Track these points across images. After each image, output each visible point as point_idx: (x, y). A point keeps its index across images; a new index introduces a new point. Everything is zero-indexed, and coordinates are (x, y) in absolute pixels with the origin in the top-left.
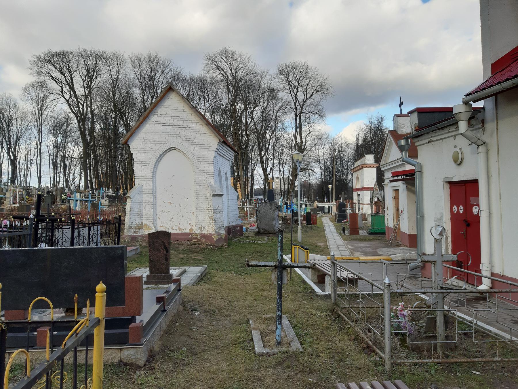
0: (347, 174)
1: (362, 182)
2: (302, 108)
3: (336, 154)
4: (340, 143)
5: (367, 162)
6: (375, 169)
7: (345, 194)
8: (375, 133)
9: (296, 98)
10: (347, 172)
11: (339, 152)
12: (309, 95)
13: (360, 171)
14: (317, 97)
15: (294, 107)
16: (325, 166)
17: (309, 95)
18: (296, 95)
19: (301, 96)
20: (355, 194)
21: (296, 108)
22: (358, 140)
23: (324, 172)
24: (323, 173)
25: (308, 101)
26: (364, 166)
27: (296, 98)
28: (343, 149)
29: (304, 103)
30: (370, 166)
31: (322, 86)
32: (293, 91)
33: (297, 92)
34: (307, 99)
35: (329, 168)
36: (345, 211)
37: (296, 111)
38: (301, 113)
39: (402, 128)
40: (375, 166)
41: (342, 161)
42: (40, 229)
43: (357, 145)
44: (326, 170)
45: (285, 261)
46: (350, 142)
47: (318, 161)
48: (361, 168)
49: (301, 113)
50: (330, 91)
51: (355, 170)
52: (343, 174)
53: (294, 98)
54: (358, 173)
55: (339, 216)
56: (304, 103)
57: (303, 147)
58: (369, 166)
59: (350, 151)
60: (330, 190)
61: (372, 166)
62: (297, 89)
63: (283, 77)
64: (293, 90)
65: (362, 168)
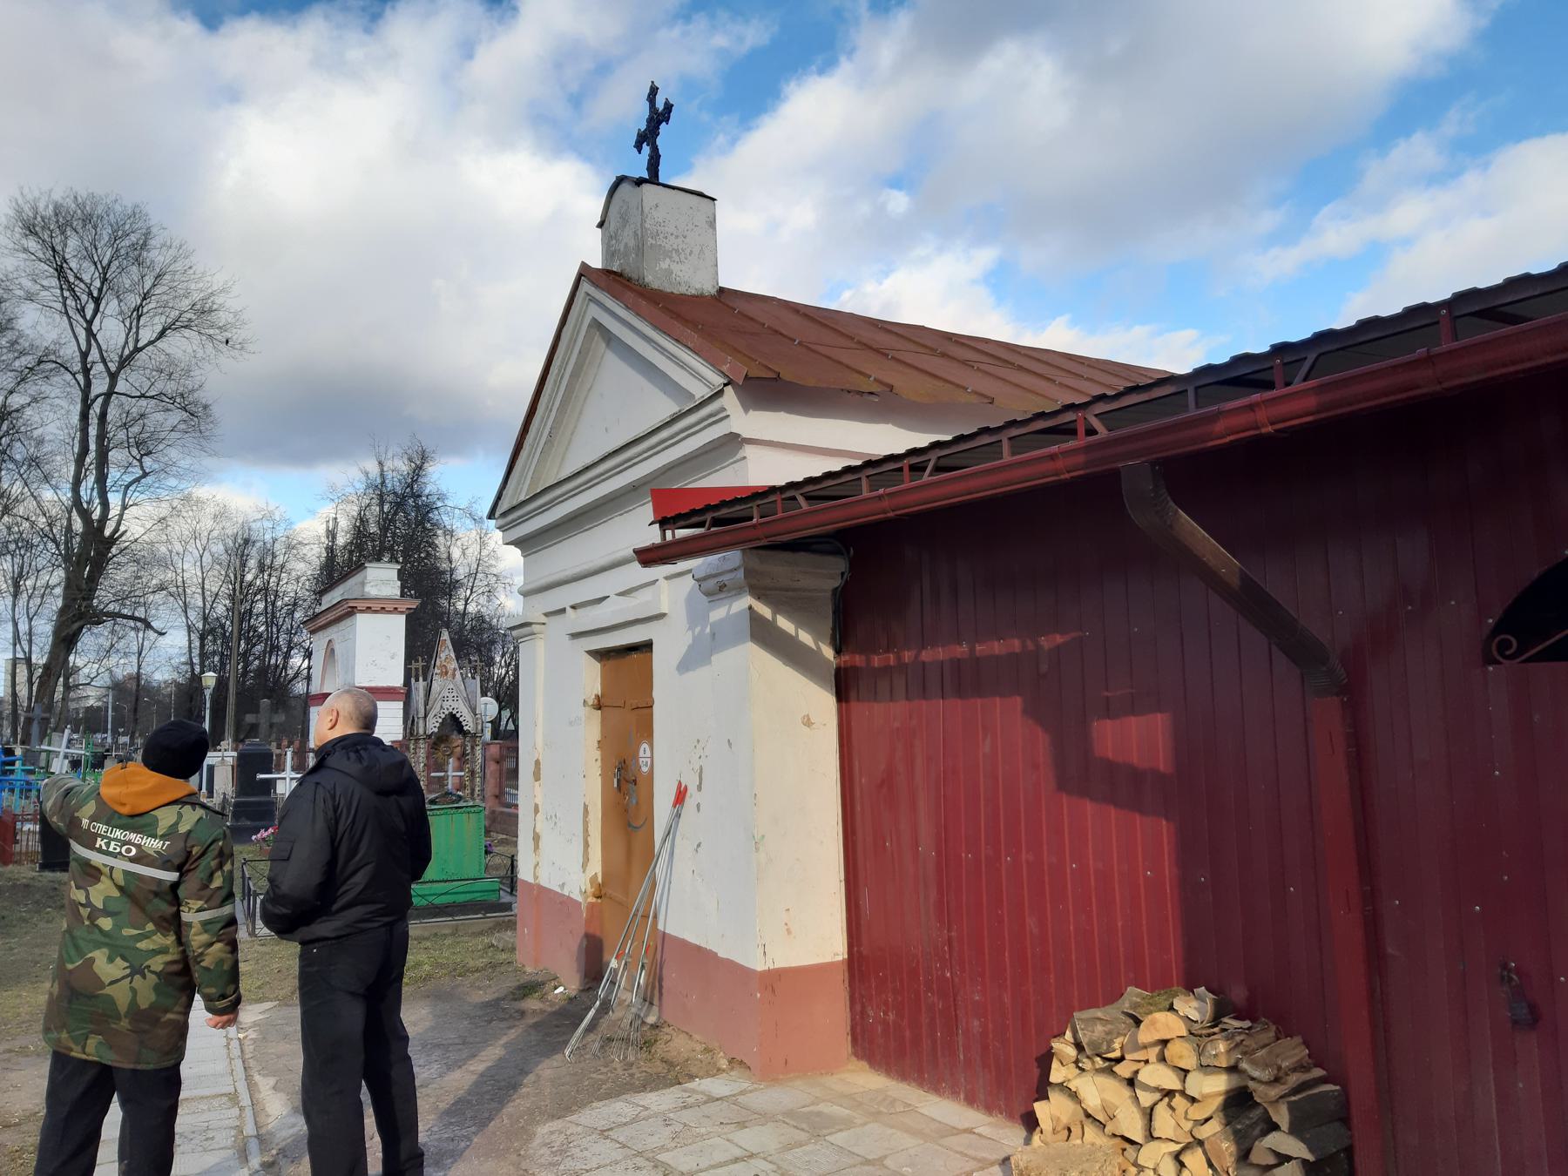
0: (290, 648)
1: (350, 669)
2: (113, 377)
3: (249, 577)
4: (268, 537)
5: (371, 590)
6: (400, 621)
7: (275, 709)
8: (400, 504)
9: (91, 334)
10: (290, 641)
11: (262, 568)
12: (146, 335)
13: (348, 622)
14: (179, 346)
15: (77, 367)
16: (205, 618)
17: (146, 335)
18: (90, 323)
19: (111, 331)
20: (719, 380)
21: (86, 371)
22: (332, 534)
23: (202, 638)
24: (197, 643)
25: (141, 356)
26: (361, 605)
27: (91, 334)
28: (280, 560)
29: (125, 362)
30: (379, 607)
31: (203, 311)
32: (81, 311)
33: (96, 311)
34: (137, 350)
35: (223, 626)
36: (270, 784)
37: (88, 384)
38: (108, 395)
39: (667, 254)
40: (402, 608)
41: (273, 604)
42: (972, 650)
43: (330, 550)
44: (208, 631)
45: (107, 899)
46: (305, 536)
47: (181, 593)
48: (347, 611)
49: (108, 395)
50: (236, 335)
51: (322, 621)
52: (275, 648)
53: (82, 335)
54: (332, 633)
55: (240, 810)
56: (125, 362)
57: (107, 533)
58: (376, 606)
59: (303, 568)
60: (208, 693)
61: (389, 607)
62: (97, 301)
63: (32, 244)
64: (82, 300)
65: (352, 612)
